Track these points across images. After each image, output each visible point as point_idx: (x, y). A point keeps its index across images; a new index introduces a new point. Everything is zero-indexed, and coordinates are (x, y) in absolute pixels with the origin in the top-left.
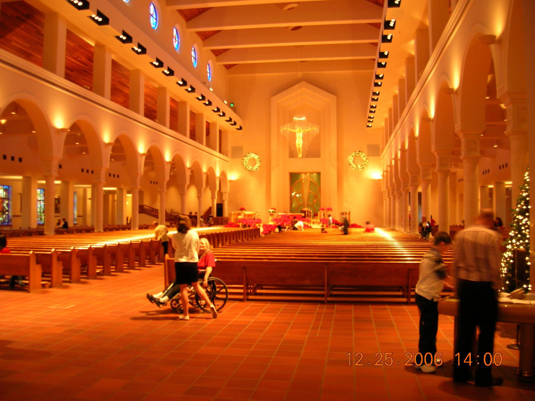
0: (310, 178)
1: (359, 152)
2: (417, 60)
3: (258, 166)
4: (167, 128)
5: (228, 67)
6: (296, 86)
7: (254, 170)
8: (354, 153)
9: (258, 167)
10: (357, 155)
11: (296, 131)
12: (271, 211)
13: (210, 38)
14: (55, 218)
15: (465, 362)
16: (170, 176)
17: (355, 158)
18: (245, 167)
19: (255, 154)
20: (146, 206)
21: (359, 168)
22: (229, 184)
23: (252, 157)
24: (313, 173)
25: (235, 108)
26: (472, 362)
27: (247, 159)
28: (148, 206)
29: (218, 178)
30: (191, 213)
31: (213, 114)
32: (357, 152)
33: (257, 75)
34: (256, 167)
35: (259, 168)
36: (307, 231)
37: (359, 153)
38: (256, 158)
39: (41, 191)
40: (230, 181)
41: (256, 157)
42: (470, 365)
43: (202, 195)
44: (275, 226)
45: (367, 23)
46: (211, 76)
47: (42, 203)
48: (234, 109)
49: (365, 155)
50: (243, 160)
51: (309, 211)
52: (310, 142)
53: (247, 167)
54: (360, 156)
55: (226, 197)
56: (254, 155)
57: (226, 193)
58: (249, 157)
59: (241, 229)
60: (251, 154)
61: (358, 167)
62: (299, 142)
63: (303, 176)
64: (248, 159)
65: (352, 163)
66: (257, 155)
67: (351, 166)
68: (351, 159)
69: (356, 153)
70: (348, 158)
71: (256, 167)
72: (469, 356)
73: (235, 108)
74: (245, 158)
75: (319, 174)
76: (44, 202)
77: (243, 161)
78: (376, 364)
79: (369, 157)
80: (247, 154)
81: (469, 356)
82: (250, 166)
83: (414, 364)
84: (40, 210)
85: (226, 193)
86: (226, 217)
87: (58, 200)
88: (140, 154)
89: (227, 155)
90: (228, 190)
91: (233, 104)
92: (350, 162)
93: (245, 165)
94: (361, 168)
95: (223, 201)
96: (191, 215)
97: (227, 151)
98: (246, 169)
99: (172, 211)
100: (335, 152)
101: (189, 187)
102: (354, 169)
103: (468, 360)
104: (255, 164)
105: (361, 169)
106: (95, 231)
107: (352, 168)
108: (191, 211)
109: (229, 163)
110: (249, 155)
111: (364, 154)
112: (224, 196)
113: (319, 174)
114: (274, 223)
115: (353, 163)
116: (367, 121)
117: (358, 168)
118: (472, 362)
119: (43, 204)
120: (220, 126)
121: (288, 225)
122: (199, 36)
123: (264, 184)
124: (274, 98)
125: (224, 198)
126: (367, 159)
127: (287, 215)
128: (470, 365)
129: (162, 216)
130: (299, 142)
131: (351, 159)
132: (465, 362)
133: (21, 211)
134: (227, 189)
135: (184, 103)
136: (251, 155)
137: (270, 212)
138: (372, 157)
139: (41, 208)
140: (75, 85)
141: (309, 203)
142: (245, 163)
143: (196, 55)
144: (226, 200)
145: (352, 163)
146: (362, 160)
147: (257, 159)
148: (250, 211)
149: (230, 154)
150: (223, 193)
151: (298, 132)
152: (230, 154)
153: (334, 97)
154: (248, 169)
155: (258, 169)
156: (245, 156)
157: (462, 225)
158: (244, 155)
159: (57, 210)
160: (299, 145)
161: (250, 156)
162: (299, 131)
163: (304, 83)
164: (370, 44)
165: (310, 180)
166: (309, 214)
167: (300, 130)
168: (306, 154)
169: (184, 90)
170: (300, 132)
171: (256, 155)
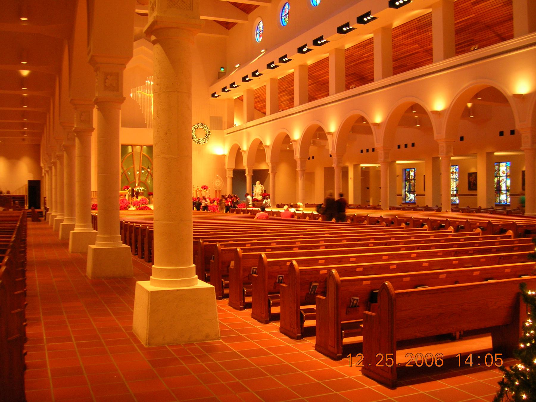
2: (504, 57)
8: (197, 125)
15: (466, 363)
26: (473, 363)
28: (95, 190)
36: (47, 182)
42: (471, 365)
45: (229, 2)
49: (208, 128)
72: (470, 357)
78: (377, 365)
79: (212, 130)
81: (470, 357)
83: (415, 365)
94: (204, 141)
103: (469, 361)
105: (204, 143)
118: (473, 363)
126: (209, 132)
128: (471, 365)
132: (466, 363)
138: (215, 131)
140: (338, 95)
164: (213, 21)
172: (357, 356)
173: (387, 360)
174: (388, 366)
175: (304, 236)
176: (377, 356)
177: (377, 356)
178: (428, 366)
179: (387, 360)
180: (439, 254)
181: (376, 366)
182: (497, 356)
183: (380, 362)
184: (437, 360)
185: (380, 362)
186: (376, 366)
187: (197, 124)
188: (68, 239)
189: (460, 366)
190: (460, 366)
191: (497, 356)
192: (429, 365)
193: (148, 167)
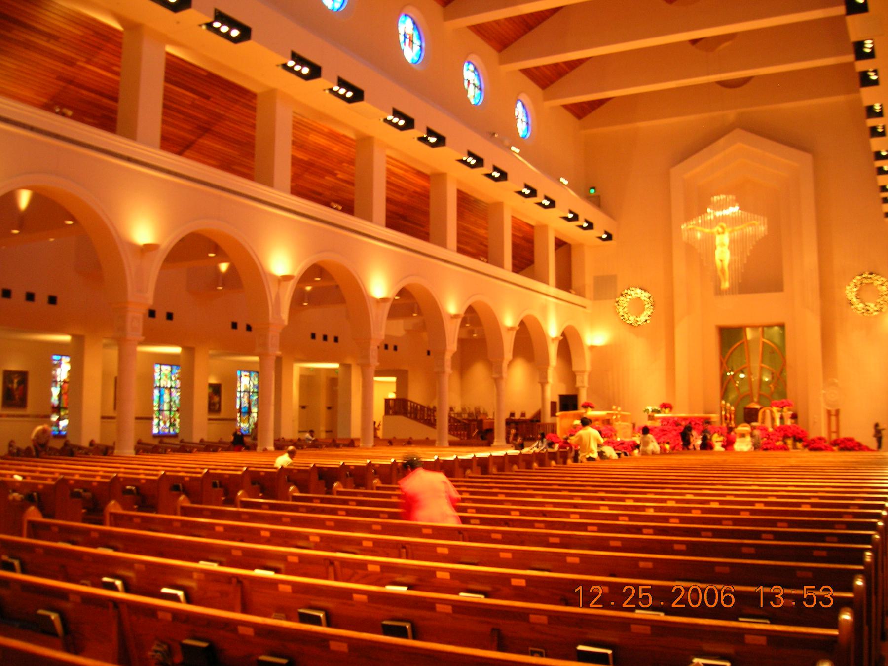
0: (763, 337)
1: (871, 274)
3: (649, 313)
4: (378, 224)
5: (581, 111)
6: (721, 142)
7: (639, 323)
8: (859, 278)
9: (649, 316)
10: (865, 281)
11: (715, 230)
12: (650, 410)
13: (513, 45)
14: (209, 424)
16: (461, 342)
17: (860, 287)
18: (622, 318)
19: (641, 289)
20: (411, 402)
21: (871, 310)
22: (588, 355)
23: (634, 296)
24: (770, 326)
25: (599, 197)
27: (625, 300)
29: (553, 340)
30: (512, 415)
31: (524, 202)
32: (864, 276)
33: (642, 125)
34: (643, 318)
35: (650, 318)
37: (870, 276)
38: (643, 299)
39: (172, 369)
40: (592, 348)
41: (644, 296)
43: (504, 375)
44: (631, 443)
46: (530, 128)
47: (176, 395)
48: (597, 202)
50: (617, 302)
51: (727, 408)
52: (749, 254)
53: (626, 316)
54: (872, 283)
55: (582, 382)
56: (638, 291)
57: (583, 372)
58: (630, 297)
59: (501, 450)
60: (634, 289)
61: (868, 308)
62: (723, 255)
63: (750, 334)
64: (628, 300)
65: (855, 300)
66: (645, 291)
67: (853, 307)
68: (850, 291)
69: (864, 276)
70: (845, 290)
71: (643, 318)
73: (599, 197)
74: (622, 298)
75: (782, 326)
76: (258, 395)
77: (616, 304)
80: (626, 291)
82: (632, 315)
84: (171, 407)
85: (583, 372)
86: (548, 424)
87: (216, 389)
88: (273, 277)
89: (581, 294)
90: (588, 367)
91: (594, 188)
92: (849, 298)
93: (621, 313)
95: (577, 389)
96: (513, 418)
97: (584, 286)
98: (623, 321)
99: (478, 412)
100: (816, 275)
101: (510, 363)
102: (859, 312)
104: (643, 310)
106: (258, 448)
107: (854, 311)
108: (513, 410)
109: (588, 311)
110: (629, 292)
111: (882, 279)
112: (578, 378)
113: (782, 326)
114: (743, 435)
115: (857, 299)
116: (880, 201)
117: (868, 310)
119: (179, 394)
120: (556, 231)
121: (668, 440)
122: (482, 39)
123: (662, 352)
124: (674, 171)
125: (578, 384)
127: (673, 418)
129: (444, 422)
130: (723, 255)
131: (850, 291)
133: (115, 408)
134: (584, 364)
135: (440, 177)
136: (632, 293)
137: (647, 411)
139: (172, 403)
141: (762, 392)
142: (621, 309)
143: (482, 79)
144: (584, 387)
145: (855, 300)
146: (878, 291)
147: (646, 299)
148: (628, 412)
149: (589, 291)
150: (577, 374)
151: (719, 234)
152: (589, 291)
153: (808, 157)
154: (628, 322)
155: (648, 322)
156: (622, 295)
157: (574, 430)
158: (619, 293)
159: (214, 407)
160: (721, 261)
161: (631, 295)
162: (720, 230)
163: (738, 132)
165: (763, 343)
166: (728, 416)
167: (722, 228)
168: (740, 281)
169: (416, 139)
170: (723, 233)
171: (643, 292)
172: (821, 590)
173: (641, 596)
174: (807, 606)
175: (321, 502)
176: (624, 590)
177: (624, 590)
178: (709, 606)
179: (641, 596)
180: (328, 523)
181: (623, 606)
182: (643, 589)
183: (629, 599)
184: (724, 597)
185: (629, 599)
186: (623, 606)
187: (860, 276)
188: (157, 513)
189: (762, 606)
190: (762, 606)
191: (643, 589)
192: (711, 605)
193: (880, 285)
